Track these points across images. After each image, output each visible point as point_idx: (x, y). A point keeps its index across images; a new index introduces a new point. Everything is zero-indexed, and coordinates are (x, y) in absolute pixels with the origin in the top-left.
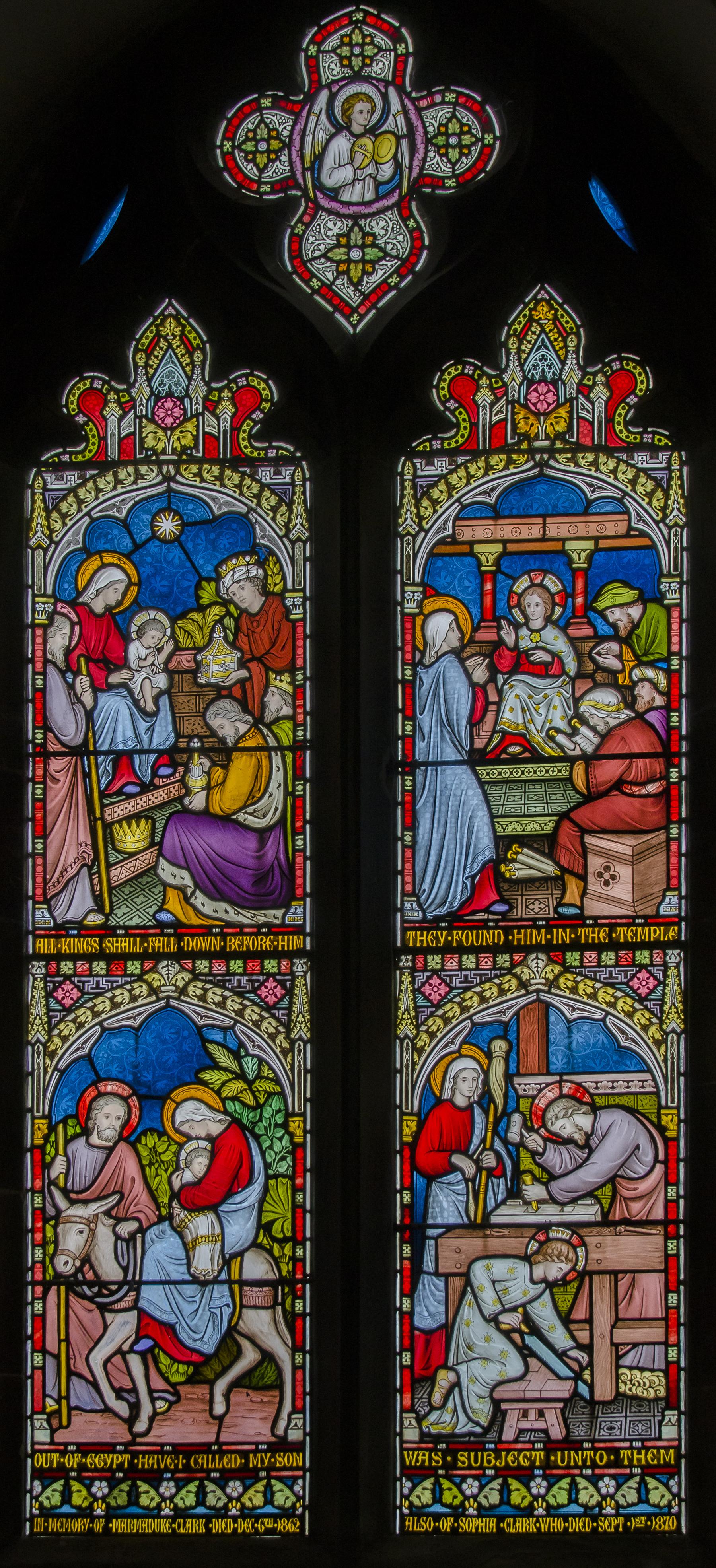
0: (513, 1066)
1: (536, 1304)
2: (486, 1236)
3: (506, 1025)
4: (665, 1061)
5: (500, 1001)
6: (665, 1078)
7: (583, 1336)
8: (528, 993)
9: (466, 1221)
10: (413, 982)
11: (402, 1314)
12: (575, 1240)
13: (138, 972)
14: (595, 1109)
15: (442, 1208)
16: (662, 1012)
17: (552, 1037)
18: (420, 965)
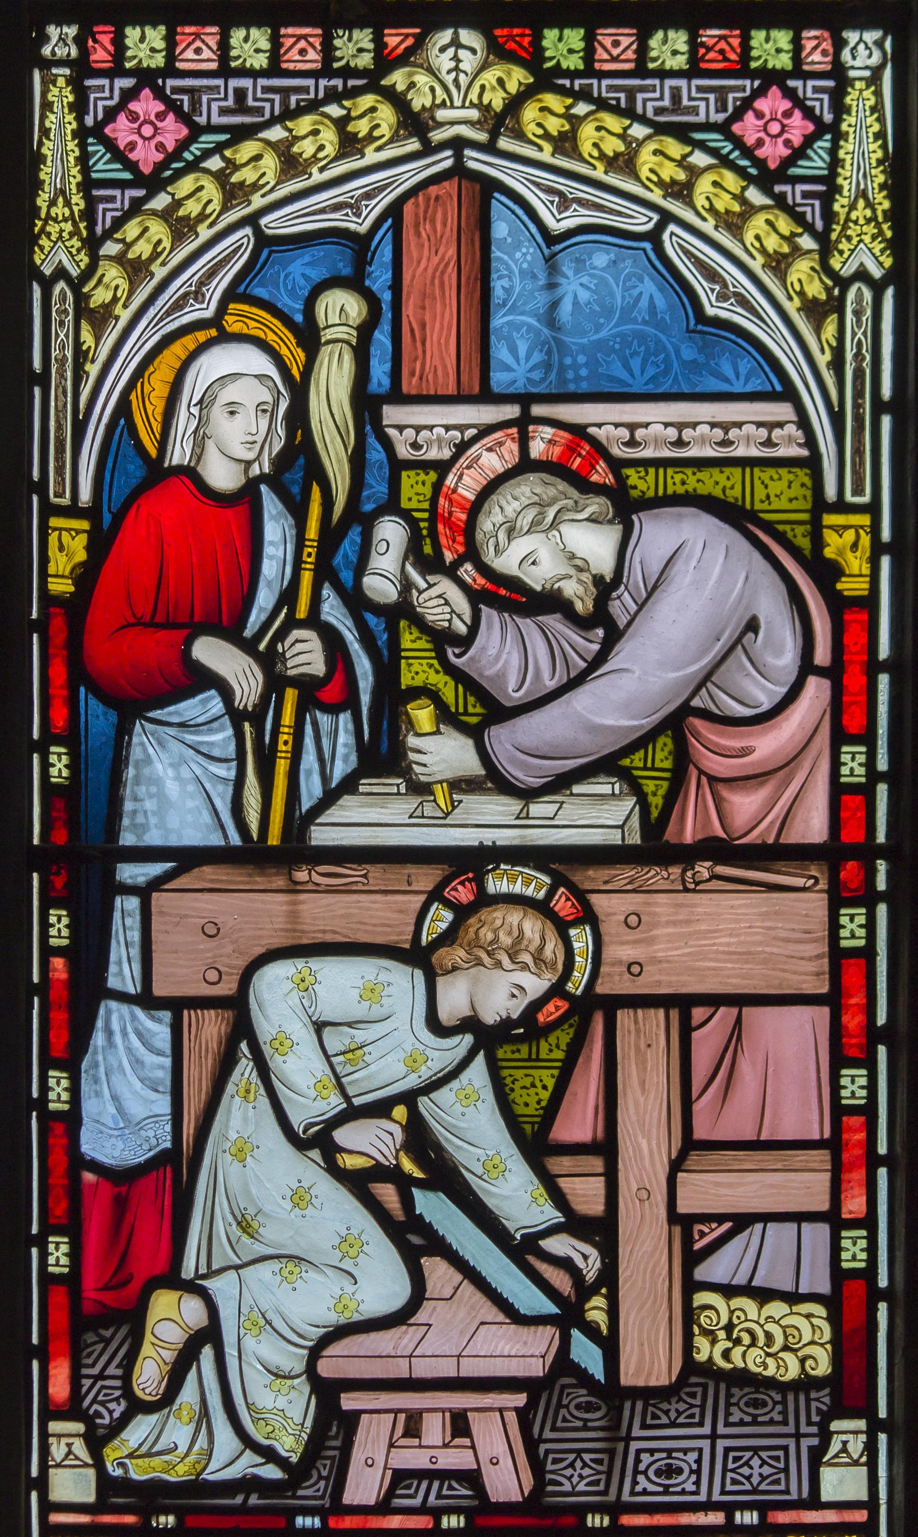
0: (380, 372)
1: (444, 1095)
2: (294, 888)
3: (360, 246)
4: (837, 364)
5: (333, 170)
6: (837, 419)
7: (587, 1194)
8: (428, 149)
9: (235, 839)
10: (79, 107)
11: (47, 1118)
12: (563, 904)
14: (626, 508)
15: (161, 796)
17: (498, 287)
18: (100, 56)
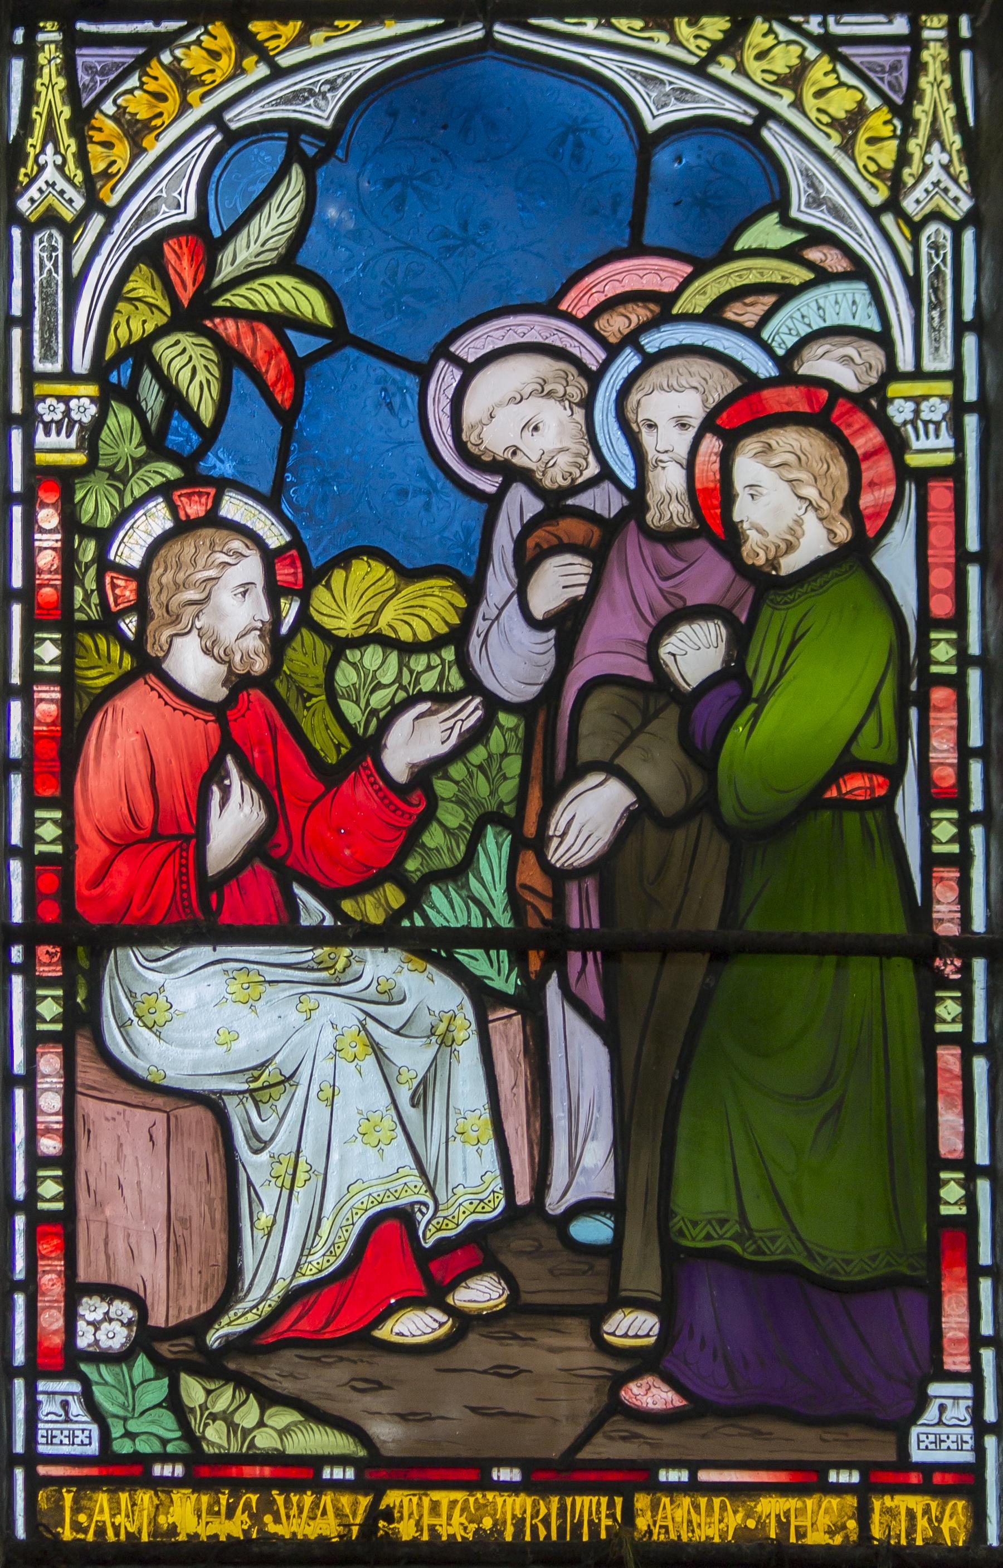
6: (913, 285)
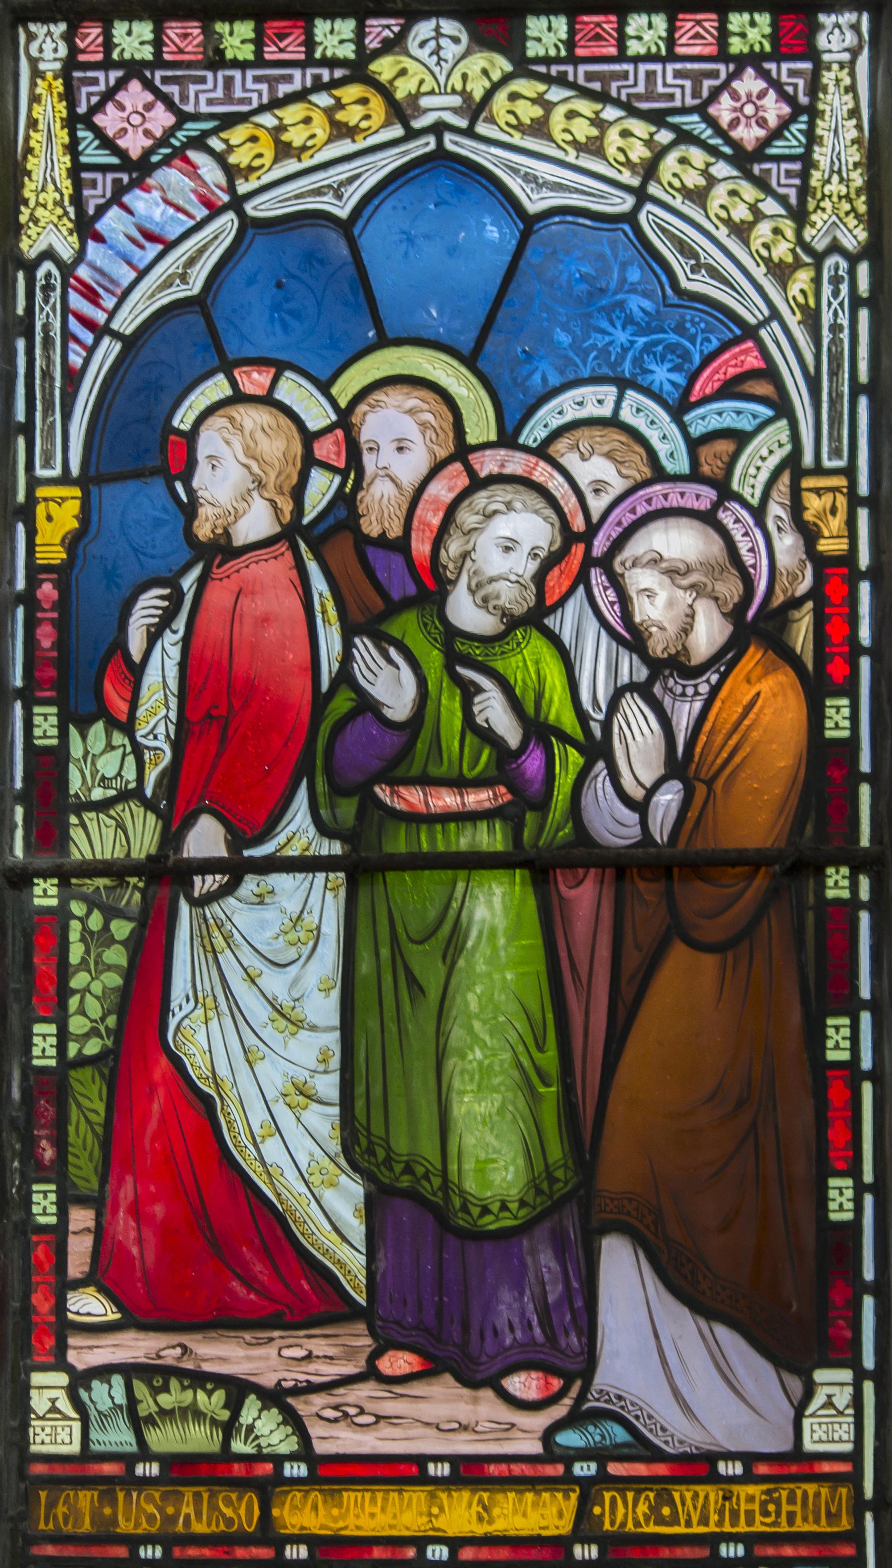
6: (813, 384)
8: (411, 134)
10: (70, 96)
13: (348, 52)
16: (804, 191)
